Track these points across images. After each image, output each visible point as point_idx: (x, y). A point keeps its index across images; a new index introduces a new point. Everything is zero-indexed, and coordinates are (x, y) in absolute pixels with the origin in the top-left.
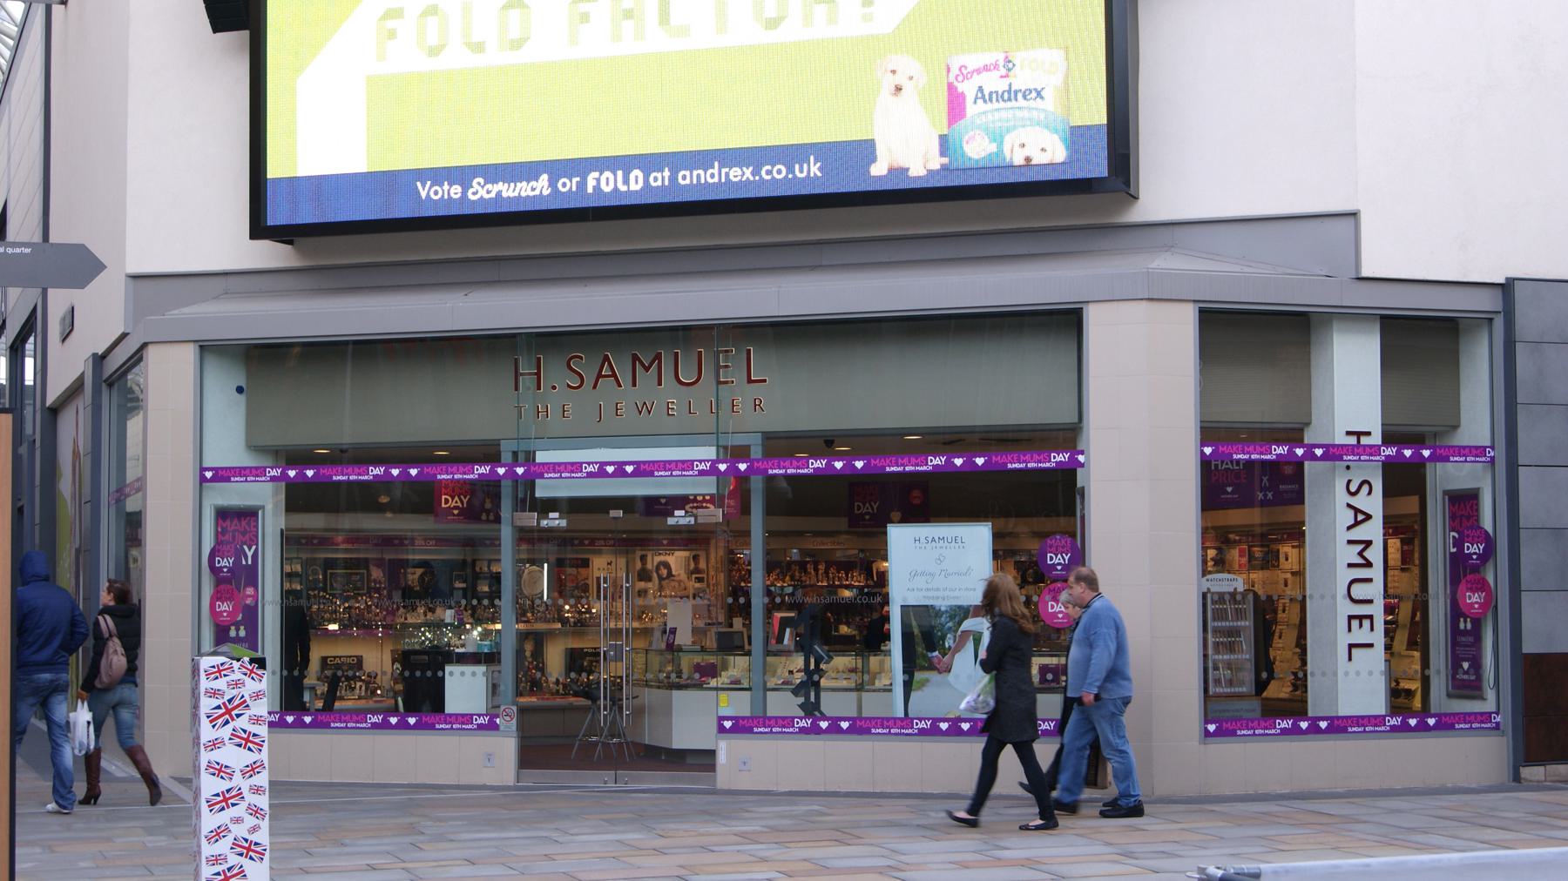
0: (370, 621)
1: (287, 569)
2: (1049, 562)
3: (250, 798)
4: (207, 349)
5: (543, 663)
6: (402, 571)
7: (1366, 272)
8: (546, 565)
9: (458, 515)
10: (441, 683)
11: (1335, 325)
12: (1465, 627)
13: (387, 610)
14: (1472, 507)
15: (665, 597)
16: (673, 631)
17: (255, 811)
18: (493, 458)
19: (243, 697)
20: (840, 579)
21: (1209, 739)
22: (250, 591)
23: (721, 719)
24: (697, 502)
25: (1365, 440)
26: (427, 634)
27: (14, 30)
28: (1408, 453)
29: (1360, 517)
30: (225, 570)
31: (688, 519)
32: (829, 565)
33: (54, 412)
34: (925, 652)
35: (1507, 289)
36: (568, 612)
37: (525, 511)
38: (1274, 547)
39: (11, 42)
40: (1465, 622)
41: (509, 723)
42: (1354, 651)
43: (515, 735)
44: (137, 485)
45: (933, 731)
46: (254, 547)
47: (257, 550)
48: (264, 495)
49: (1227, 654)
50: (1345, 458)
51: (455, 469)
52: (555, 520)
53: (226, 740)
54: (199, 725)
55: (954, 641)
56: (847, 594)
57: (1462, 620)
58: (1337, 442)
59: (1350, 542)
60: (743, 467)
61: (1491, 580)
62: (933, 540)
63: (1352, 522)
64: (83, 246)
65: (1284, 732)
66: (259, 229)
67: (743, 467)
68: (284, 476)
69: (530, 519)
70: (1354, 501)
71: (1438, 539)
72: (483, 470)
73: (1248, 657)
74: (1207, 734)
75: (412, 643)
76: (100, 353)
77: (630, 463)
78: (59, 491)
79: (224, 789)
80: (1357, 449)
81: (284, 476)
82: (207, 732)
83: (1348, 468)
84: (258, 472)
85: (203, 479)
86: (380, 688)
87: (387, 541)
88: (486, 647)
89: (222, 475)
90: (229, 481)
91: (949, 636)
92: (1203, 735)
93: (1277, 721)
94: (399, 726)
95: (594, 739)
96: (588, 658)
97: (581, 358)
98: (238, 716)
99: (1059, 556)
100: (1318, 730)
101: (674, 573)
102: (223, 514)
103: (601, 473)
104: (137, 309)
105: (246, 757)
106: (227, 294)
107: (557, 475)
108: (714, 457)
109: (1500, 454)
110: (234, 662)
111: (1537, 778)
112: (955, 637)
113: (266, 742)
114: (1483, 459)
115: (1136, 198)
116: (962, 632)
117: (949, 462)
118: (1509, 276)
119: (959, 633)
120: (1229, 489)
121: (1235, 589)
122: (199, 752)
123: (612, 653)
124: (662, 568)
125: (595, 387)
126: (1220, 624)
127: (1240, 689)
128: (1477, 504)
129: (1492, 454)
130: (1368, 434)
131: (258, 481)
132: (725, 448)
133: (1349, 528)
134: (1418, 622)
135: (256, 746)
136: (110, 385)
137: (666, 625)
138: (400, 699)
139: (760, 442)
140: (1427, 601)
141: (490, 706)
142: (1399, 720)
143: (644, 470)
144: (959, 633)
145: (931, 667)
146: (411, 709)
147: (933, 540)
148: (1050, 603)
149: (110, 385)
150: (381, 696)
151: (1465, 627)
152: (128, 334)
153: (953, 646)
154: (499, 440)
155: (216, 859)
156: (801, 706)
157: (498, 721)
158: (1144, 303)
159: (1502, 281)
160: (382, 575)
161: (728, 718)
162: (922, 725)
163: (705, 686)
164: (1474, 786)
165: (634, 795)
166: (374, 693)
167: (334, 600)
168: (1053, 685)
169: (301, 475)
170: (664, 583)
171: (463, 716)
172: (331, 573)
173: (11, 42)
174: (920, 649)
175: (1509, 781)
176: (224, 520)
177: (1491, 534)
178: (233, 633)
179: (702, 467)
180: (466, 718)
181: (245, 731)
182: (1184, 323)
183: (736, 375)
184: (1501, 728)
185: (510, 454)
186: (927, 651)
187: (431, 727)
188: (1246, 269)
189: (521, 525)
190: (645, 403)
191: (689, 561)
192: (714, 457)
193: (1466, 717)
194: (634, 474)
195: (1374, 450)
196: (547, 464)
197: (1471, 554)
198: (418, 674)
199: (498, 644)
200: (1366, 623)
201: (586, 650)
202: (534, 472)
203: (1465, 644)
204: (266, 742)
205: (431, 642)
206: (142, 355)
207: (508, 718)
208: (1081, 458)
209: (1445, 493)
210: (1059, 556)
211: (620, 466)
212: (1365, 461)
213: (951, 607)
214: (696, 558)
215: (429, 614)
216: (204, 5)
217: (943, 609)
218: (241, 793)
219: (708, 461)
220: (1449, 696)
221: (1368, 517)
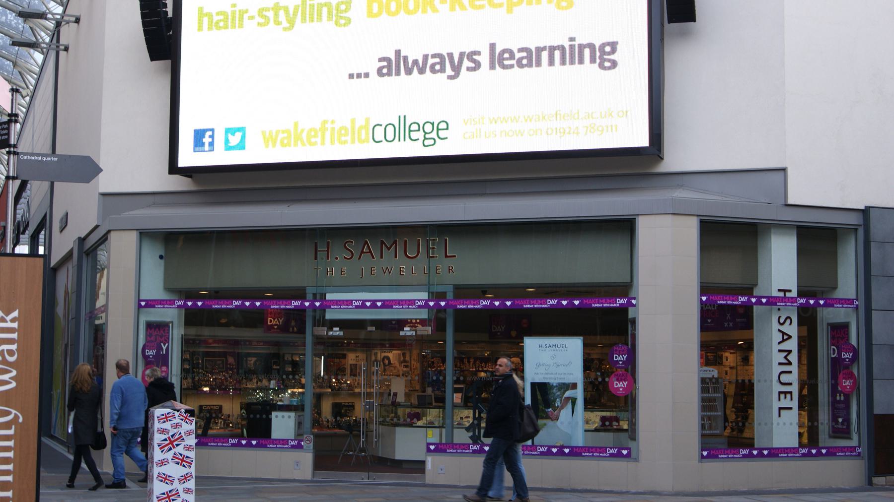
0: (227, 386)
2: (615, 359)
4: (145, 235)
5: (320, 411)
6: (245, 359)
7: (790, 202)
8: (323, 357)
9: (277, 329)
10: (269, 421)
11: (773, 231)
12: (840, 399)
13: (236, 380)
14: (844, 333)
15: (387, 375)
16: (395, 394)
18: (303, 298)
19: (180, 433)
20: (482, 367)
21: (704, 460)
23: (429, 444)
24: (413, 323)
25: (788, 295)
26: (260, 394)
27: (37, 70)
28: (812, 302)
29: (785, 337)
30: (151, 357)
31: (412, 332)
32: (476, 359)
33: (55, 270)
34: (544, 408)
35: (866, 212)
36: (335, 383)
37: (319, 326)
38: (720, 353)
39: (36, 76)
40: (840, 396)
41: (308, 444)
42: (782, 412)
43: (312, 451)
44: (102, 309)
45: (548, 453)
46: (167, 344)
47: (168, 346)
48: (170, 315)
49: (709, 412)
50: (778, 304)
51: (281, 303)
52: (336, 332)
53: (170, 460)
54: (153, 451)
55: (561, 403)
56: (483, 374)
57: (838, 395)
58: (773, 295)
59: (780, 351)
60: (443, 304)
61: (856, 373)
62: (550, 346)
63: (781, 340)
64: (89, 157)
65: (744, 456)
66: (174, 168)
67: (443, 304)
68: (185, 304)
69: (323, 331)
70: (782, 328)
71: (825, 351)
72: (297, 303)
73: (720, 413)
74: (703, 457)
75: (252, 399)
76: (82, 237)
77: (379, 301)
78: (57, 313)
79: (168, 490)
80: (784, 299)
81: (185, 304)
83: (779, 309)
84: (171, 302)
85: (140, 306)
86: (231, 423)
87: (236, 343)
88: (295, 401)
89: (151, 304)
90: (154, 307)
91: (558, 400)
92: (700, 458)
93: (741, 450)
94: (246, 445)
95: (351, 453)
96: (344, 408)
97: (352, 242)
98: (177, 445)
99: (621, 356)
100: (762, 455)
101: (392, 362)
103: (363, 306)
104: (104, 212)
105: (182, 471)
106: (155, 205)
107: (338, 307)
108: (427, 298)
109: (861, 303)
110: (176, 412)
111: (881, 484)
112: (561, 400)
113: (194, 461)
114: (852, 306)
115: (662, 159)
116: (565, 398)
117: (559, 303)
118: (867, 205)
119: (563, 398)
120: (709, 321)
121: (713, 376)
122: (153, 467)
123: (367, 406)
124: (385, 359)
125: (359, 258)
126: (705, 395)
127: (716, 432)
128: (848, 331)
129: (857, 303)
130: (790, 291)
131: (170, 308)
132: (433, 293)
133: (779, 343)
134: (805, 396)
135: (187, 464)
136: (88, 255)
137: (390, 391)
138: (245, 430)
139: (452, 290)
140: (817, 385)
141: (296, 435)
142: (807, 450)
143: (387, 304)
144: (563, 398)
145: (547, 417)
146: (251, 436)
147: (550, 346)
148: (615, 382)
149: (88, 255)
150: (232, 427)
151: (840, 399)
152: (99, 226)
153: (560, 405)
154: (305, 287)
156: (471, 438)
157: (302, 443)
158: (670, 215)
159: (863, 208)
160: (233, 361)
161: (432, 444)
162: (542, 449)
163: (414, 425)
164: (847, 487)
165: (380, 487)
166: (228, 425)
167: (207, 374)
168: (609, 428)
169: (195, 305)
170: (387, 367)
171: (283, 440)
172: (206, 360)
173: (24, 110)
175: (866, 485)
176: (151, 329)
177: (856, 347)
179: (420, 303)
180: (284, 442)
181: (181, 455)
182: (691, 229)
183: (439, 254)
184: (862, 455)
185: (312, 295)
186: (545, 408)
187: (265, 446)
188: (724, 199)
189: (318, 334)
190: (387, 268)
191: (400, 356)
192: (427, 298)
193: (842, 449)
195: (793, 300)
196: (333, 300)
197: (845, 358)
198: (258, 416)
199: (302, 401)
200: (788, 396)
201: (343, 404)
202: (326, 305)
203: (839, 408)
204: (194, 461)
205: (262, 398)
206: (107, 237)
207: (308, 442)
208: (634, 302)
209: (828, 324)
210: (621, 356)
211: (374, 302)
212: (789, 306)
213: (559, 384)
214: (404, 354)
215: (259, 383)
216: (146, 46)
217: (555, 385)
218: (178, 493)
219: (423, 300)
220: (830, 437)
221: (790, 337)
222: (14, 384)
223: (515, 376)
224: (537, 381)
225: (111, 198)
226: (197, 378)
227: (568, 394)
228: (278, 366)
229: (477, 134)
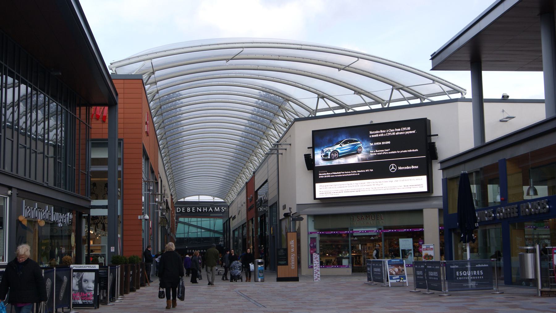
1: (320, 246)
4: (308, 216)
17: (318, 267)
22: (315, 249)
41: (350, 266)
48: (316, 236)
52: (356, 238)
66: (315, 198)
67: (380, 231)
69: (353, 238)
82: (314, 260)
84: (316, 232)
85: (308, 234)
89: (311, 233)
103: (362, 232)
143: (367, 232)
145: (405, 258)
155: (315, 271)
174: (404, 255)
180: (345, 266)
192: (376, 230)
194: (366, 232)
211: (364, 231)
222: (294, 250)
223: (532, 248)
224: (403, 249)
225: (299, 205)
226: (324, 252)
227: (410, 252)
228: (532, 246)
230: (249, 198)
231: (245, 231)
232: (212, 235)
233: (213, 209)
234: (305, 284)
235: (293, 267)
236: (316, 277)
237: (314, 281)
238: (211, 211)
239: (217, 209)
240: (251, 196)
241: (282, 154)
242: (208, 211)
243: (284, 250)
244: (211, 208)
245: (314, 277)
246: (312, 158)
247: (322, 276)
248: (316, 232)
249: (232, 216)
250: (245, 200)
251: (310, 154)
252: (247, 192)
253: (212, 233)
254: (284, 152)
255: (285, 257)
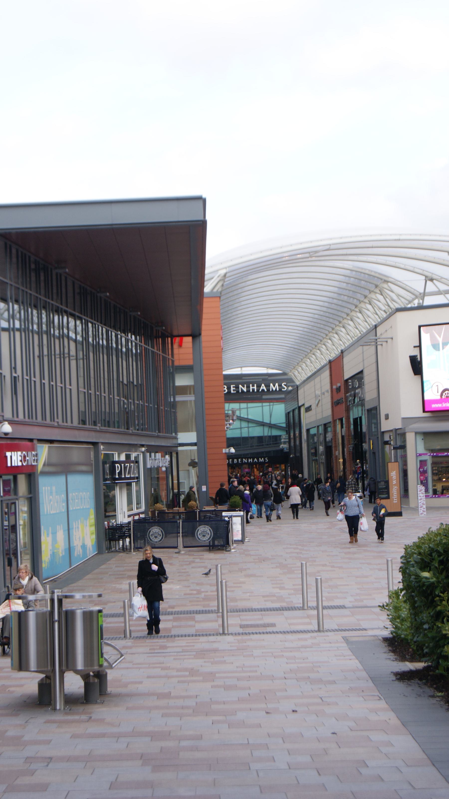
3: (423, 499)
4: (416, 433)
17: (424, 500)
48: (428, 458)
66: (424, 411)
82: (419, 493)
84: (426, 454)
85: (417, 456)
89: (420, 455)
102: (421, 462)
155: (420, 505)
178: (424, 482)
229: (174, 656)
230: (334, 387)
231: (329, 436)
232: (266, 432)
233: (268, 386)
234: (406, 520)
235: (396, 501)
236: (421, 511)
237: (419, 515)
238: (263, 390)
239: (274, 386)
240: (339, 385)
241: (382, 345)
242: (258, 391)
243: (385, 483)
244: (263, 385)
245: (420, 511)
246: (419, 359)
247: (429, 508)
248: (426, 454)
249: (303, 405)
250: (327, 387)
251: (417, 356)
252: (331, 375)
253: (266, 429)
254: (384, 344)
255: (386, 490)
